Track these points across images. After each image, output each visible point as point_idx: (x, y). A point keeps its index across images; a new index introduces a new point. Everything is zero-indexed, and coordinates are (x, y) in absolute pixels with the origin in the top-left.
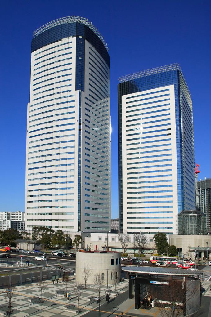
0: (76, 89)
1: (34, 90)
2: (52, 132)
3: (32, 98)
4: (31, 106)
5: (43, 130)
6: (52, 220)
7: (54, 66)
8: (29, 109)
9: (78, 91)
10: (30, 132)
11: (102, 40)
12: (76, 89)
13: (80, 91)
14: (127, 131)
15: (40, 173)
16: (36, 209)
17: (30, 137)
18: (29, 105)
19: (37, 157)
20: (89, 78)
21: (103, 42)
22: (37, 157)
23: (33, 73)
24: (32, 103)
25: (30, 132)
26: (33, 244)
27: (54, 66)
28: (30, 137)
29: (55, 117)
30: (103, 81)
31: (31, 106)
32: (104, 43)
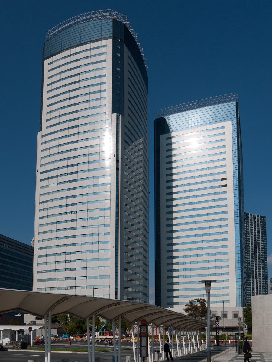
0: (113, 112)
1: (49, 85)
2: (76, 204)
3: (45, 124)
4: (43, 136)
5: (62, 240)
6: (178, 205)
7: (81, 81)
8: (40, 140)
9: (115, 115)
10: (42, 173)
11: (130, 28)
12: (113, 112)
13: (119, 115)
14: (226, 206)
15: (57, 263)
16: (61, 248)
17: (41, 180)
18: (40, 134)
19: (54, 162)
20: (125, 132)
21: (132, 31)
22: (54, 162)
23: (45, 96)
24: (44, 131)
25: (42, 173)
26: (56, 330)
27: (81, 81)
28: (41, 180)
29: (81, 143)
30: (141, 113)
31: (43, 136)
32: (132, 33)
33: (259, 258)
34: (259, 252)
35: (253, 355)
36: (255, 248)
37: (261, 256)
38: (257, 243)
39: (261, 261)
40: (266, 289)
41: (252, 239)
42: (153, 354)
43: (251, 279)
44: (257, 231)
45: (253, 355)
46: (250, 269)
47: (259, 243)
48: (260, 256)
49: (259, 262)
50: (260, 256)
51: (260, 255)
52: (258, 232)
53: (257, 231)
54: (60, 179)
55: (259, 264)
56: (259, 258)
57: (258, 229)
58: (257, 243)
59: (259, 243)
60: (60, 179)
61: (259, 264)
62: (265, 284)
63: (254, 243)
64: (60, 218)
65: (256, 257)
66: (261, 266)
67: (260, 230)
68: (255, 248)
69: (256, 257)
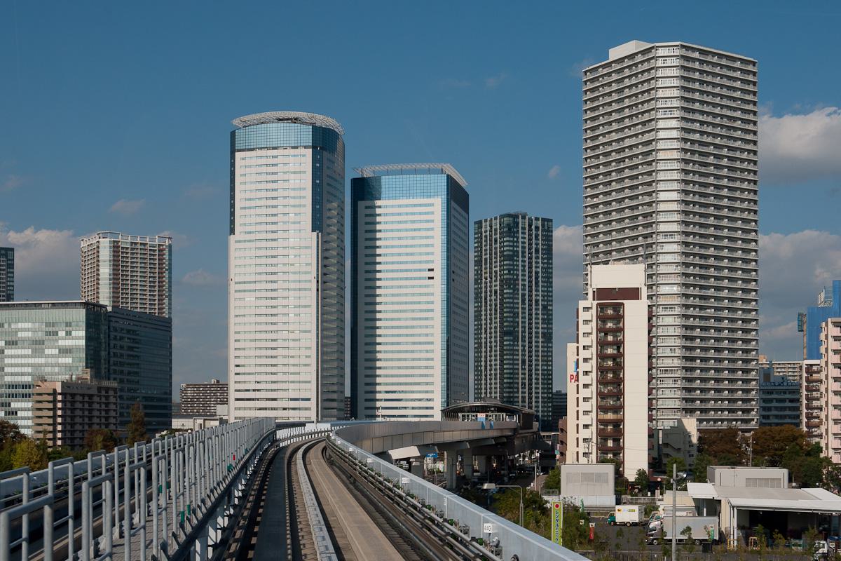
33: (537, 301)
36: (530, 282)
37: (540, 298)
39: (540, 307)
44: (533, 250)
47: (537, 273)
52: (537, 251)
55: (537, 314)
56: (537, 301)
59: (537, 273)
65: (530, 301)
66: (540, 316)
67: (540, 247)
68: (530, 282)
69: (530, 301)
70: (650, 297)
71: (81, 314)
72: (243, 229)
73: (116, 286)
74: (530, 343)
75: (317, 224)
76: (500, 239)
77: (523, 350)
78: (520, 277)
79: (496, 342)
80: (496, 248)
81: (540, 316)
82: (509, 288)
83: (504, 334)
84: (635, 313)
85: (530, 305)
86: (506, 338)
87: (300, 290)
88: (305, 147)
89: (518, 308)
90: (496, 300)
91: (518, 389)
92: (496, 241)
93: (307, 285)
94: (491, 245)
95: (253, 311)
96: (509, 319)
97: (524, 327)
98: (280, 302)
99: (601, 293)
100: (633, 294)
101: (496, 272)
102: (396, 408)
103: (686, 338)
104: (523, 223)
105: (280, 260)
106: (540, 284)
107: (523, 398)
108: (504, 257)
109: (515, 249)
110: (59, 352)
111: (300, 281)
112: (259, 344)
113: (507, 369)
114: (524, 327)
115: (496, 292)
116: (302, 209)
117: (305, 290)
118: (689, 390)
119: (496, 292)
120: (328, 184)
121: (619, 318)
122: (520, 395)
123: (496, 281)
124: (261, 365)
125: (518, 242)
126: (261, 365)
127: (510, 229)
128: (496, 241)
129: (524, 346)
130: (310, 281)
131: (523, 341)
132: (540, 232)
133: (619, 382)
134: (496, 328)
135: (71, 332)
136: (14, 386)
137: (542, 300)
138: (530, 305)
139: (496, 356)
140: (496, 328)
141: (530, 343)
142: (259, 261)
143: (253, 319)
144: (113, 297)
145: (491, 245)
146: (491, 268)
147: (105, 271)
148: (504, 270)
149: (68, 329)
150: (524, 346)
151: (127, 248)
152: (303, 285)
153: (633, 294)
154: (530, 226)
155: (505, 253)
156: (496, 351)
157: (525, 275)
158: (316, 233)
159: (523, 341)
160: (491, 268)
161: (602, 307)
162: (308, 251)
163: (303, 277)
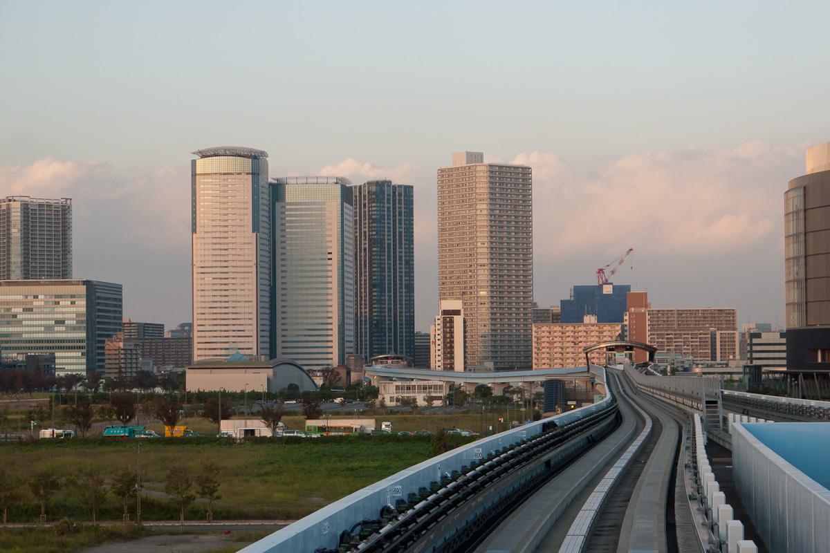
33: (401, 257)
34: (400, 248)
35: (60, 358)
36: (394, 241)
37: (403, 254)
38: (397, 233)
39: (403, 262)
40: (410, 324)
41: (389, 228)
42: (426, 544)
43: (387, 294)
44: (397, 213)
45: (60, 358)
46: (385, 276)
47: (400, 233)
48: (401, 230)
49: (400, 264)
50: (401, 230)
51: (401, 228)
52: (400, 214)
53: (397, 213)
54: (215, 276)
55: (400, 268)
56: (401, 257)
57: (400, 208)
58: (397, 233)
59: (400, 233)
60: (215, 276)
61: (400, 268)
62: (409, 300)
63: (392, 222)
64: (211, 340)
65: (395, 257)
66: (404, 270)
67: (403, 210)
68: (394, 241)
69: (395, 257)
70: (465, 314)
71: (82, 289)
72: (202, 229)
73: (26, 243)
74: (395, 293)
75: (255, 228)
76: (369, 204)
77: (390, 300)
78: (386, 237)
79: (365, 292)
80: (365, 212)
81: (404, 270)
82: (377, 247)
83: (373, 286)
84: (458, 321)
85: (395, 261)
86: (374, 290)
87: (245, 273)
88: (247, 174)
89: (385, 264)
90: (365, 256)
91: (385, 332)
92: (365, 205)
93: (250, 270)
94: (360, 209)
95: (210, 287)
96: (376, 273)
97: (389, 280)
98: (230, 281)
99: (445, 312)
100: (457, 312)
101: (365, 232)
102: (312, 353)
103: (492, 319)
104: (389, 191)
105: (230, 252)
106: (403, 242)
107: (390, 341)
108: (372, 220)
109: (382, 213)
110: (23, 311)
111: (244, 267)
112: (214, 310)
113: (375, 316)
114: (389, 280)
115: (365, 249)
116: (246, 217)
117: (248, 272)
118: (495, 347)
119: (365, 249)
120: (262, 192)
121: (452, 321)
122: (387, 339)
123: (365, 240)
124: (216, 325)
125: (384, 207)
126: (216, 325)
127: (377, 196)
128: (365, 205)
129: (390, 296)
130: (251, 267)
131: (389, 292)
132: (403, 198)
133: (452, 352)
134: (365, 280)
135: (74, 302)
136: (30, 341)
137: (405, 256)
138: (395, 261)
139: (365, 304)
140: (365, 280)
141: (395, 293)
142: (215, 252)
143: (210, 293)
144: (24, 254)
145: (360, 209)
146: (360, 229)
147: (16, 232)
148: (372, 231)
149: (72, 300)
150: (390, 296)
151: (35, 210)
152: (247, 270)
153: (457, 312)
154: (394, 193)
155: (373, 217)
156: (365, 300)
157: (390, 235)
158: (255, 234)
159: (389, 292)
160: (360, 229)
161: (444, 319)
162: (250, 246)
163: (246, 264)
